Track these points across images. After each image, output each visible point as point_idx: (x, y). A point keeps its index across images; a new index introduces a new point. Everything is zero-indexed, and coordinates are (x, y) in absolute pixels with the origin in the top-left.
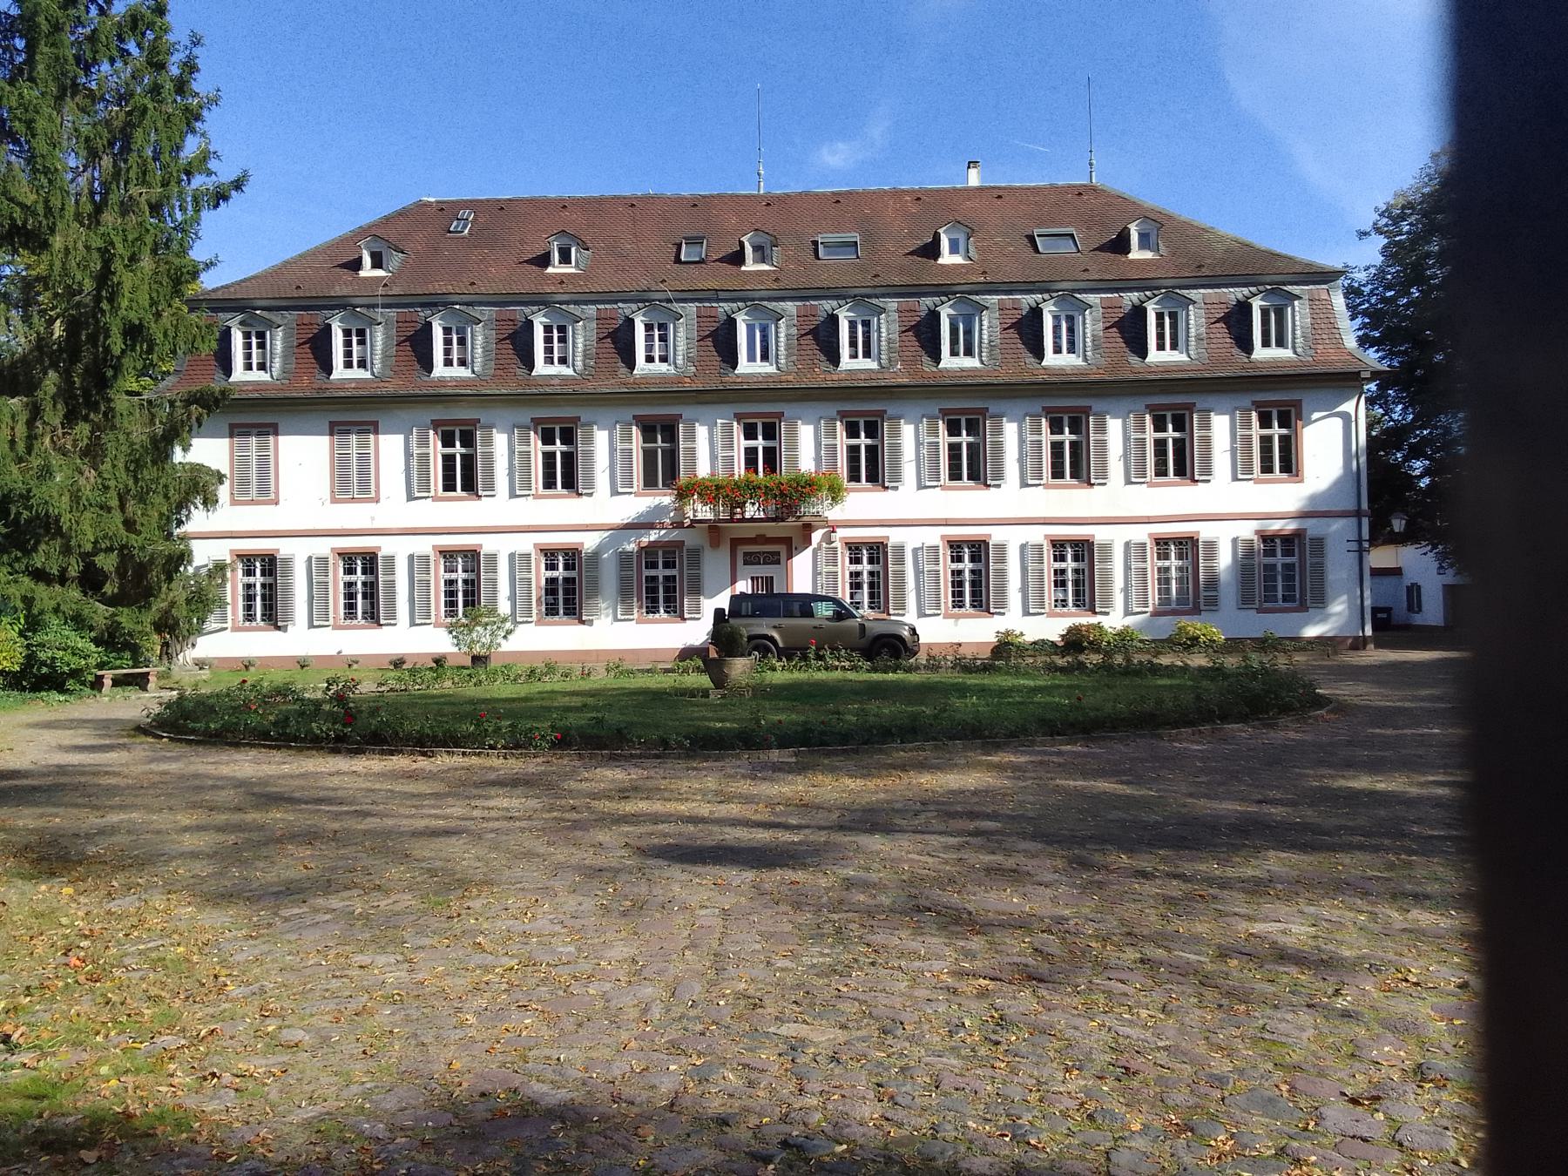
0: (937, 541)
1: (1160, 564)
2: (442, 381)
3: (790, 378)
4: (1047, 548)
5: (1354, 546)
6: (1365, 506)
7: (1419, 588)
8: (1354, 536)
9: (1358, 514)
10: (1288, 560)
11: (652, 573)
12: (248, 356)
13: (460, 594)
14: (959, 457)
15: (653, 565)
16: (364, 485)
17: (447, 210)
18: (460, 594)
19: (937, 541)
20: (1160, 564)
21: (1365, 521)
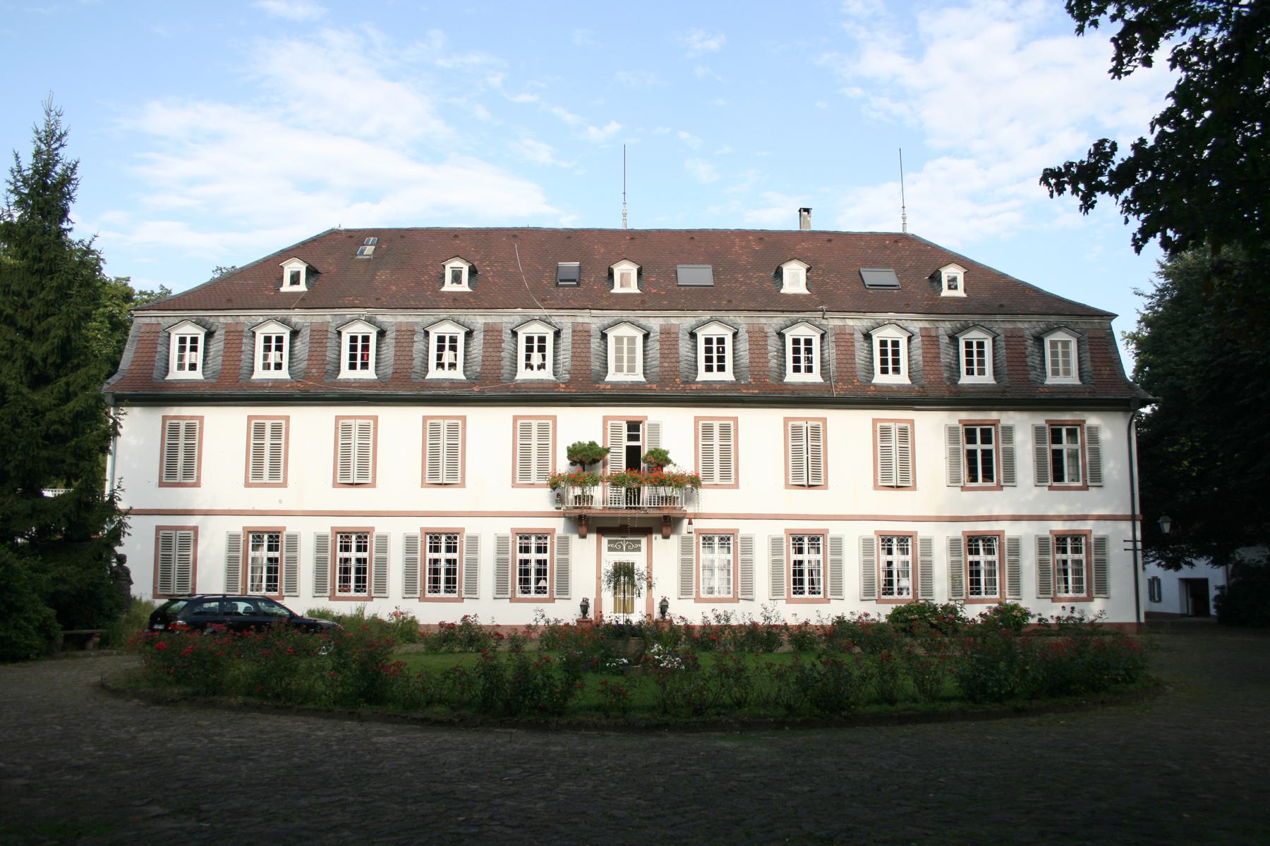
0: (782, 534)
1: (971, 558)
2: (347, 383)
3: (654, 386)
4: (877, 543)
5: (1130, 545)
6: (1137, 512)
7: (1159, 581)
8: (1130, 536)
9: (1133, 518)
10: (990, 558)
11: (346, 555)
12: (181, 358)
13: (353, 571)
14: (975, 461)
15: (346, 548)
16: (188, 472)
17: (355, 237)
18: (353, 571)
19: (782, 534)
20: (971, 558)
21: (1138, 524)
